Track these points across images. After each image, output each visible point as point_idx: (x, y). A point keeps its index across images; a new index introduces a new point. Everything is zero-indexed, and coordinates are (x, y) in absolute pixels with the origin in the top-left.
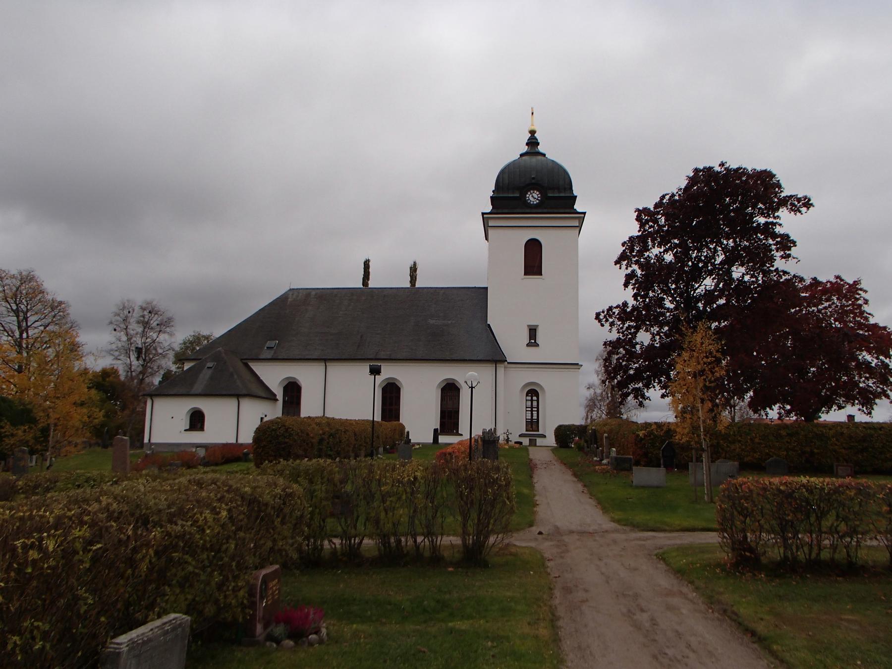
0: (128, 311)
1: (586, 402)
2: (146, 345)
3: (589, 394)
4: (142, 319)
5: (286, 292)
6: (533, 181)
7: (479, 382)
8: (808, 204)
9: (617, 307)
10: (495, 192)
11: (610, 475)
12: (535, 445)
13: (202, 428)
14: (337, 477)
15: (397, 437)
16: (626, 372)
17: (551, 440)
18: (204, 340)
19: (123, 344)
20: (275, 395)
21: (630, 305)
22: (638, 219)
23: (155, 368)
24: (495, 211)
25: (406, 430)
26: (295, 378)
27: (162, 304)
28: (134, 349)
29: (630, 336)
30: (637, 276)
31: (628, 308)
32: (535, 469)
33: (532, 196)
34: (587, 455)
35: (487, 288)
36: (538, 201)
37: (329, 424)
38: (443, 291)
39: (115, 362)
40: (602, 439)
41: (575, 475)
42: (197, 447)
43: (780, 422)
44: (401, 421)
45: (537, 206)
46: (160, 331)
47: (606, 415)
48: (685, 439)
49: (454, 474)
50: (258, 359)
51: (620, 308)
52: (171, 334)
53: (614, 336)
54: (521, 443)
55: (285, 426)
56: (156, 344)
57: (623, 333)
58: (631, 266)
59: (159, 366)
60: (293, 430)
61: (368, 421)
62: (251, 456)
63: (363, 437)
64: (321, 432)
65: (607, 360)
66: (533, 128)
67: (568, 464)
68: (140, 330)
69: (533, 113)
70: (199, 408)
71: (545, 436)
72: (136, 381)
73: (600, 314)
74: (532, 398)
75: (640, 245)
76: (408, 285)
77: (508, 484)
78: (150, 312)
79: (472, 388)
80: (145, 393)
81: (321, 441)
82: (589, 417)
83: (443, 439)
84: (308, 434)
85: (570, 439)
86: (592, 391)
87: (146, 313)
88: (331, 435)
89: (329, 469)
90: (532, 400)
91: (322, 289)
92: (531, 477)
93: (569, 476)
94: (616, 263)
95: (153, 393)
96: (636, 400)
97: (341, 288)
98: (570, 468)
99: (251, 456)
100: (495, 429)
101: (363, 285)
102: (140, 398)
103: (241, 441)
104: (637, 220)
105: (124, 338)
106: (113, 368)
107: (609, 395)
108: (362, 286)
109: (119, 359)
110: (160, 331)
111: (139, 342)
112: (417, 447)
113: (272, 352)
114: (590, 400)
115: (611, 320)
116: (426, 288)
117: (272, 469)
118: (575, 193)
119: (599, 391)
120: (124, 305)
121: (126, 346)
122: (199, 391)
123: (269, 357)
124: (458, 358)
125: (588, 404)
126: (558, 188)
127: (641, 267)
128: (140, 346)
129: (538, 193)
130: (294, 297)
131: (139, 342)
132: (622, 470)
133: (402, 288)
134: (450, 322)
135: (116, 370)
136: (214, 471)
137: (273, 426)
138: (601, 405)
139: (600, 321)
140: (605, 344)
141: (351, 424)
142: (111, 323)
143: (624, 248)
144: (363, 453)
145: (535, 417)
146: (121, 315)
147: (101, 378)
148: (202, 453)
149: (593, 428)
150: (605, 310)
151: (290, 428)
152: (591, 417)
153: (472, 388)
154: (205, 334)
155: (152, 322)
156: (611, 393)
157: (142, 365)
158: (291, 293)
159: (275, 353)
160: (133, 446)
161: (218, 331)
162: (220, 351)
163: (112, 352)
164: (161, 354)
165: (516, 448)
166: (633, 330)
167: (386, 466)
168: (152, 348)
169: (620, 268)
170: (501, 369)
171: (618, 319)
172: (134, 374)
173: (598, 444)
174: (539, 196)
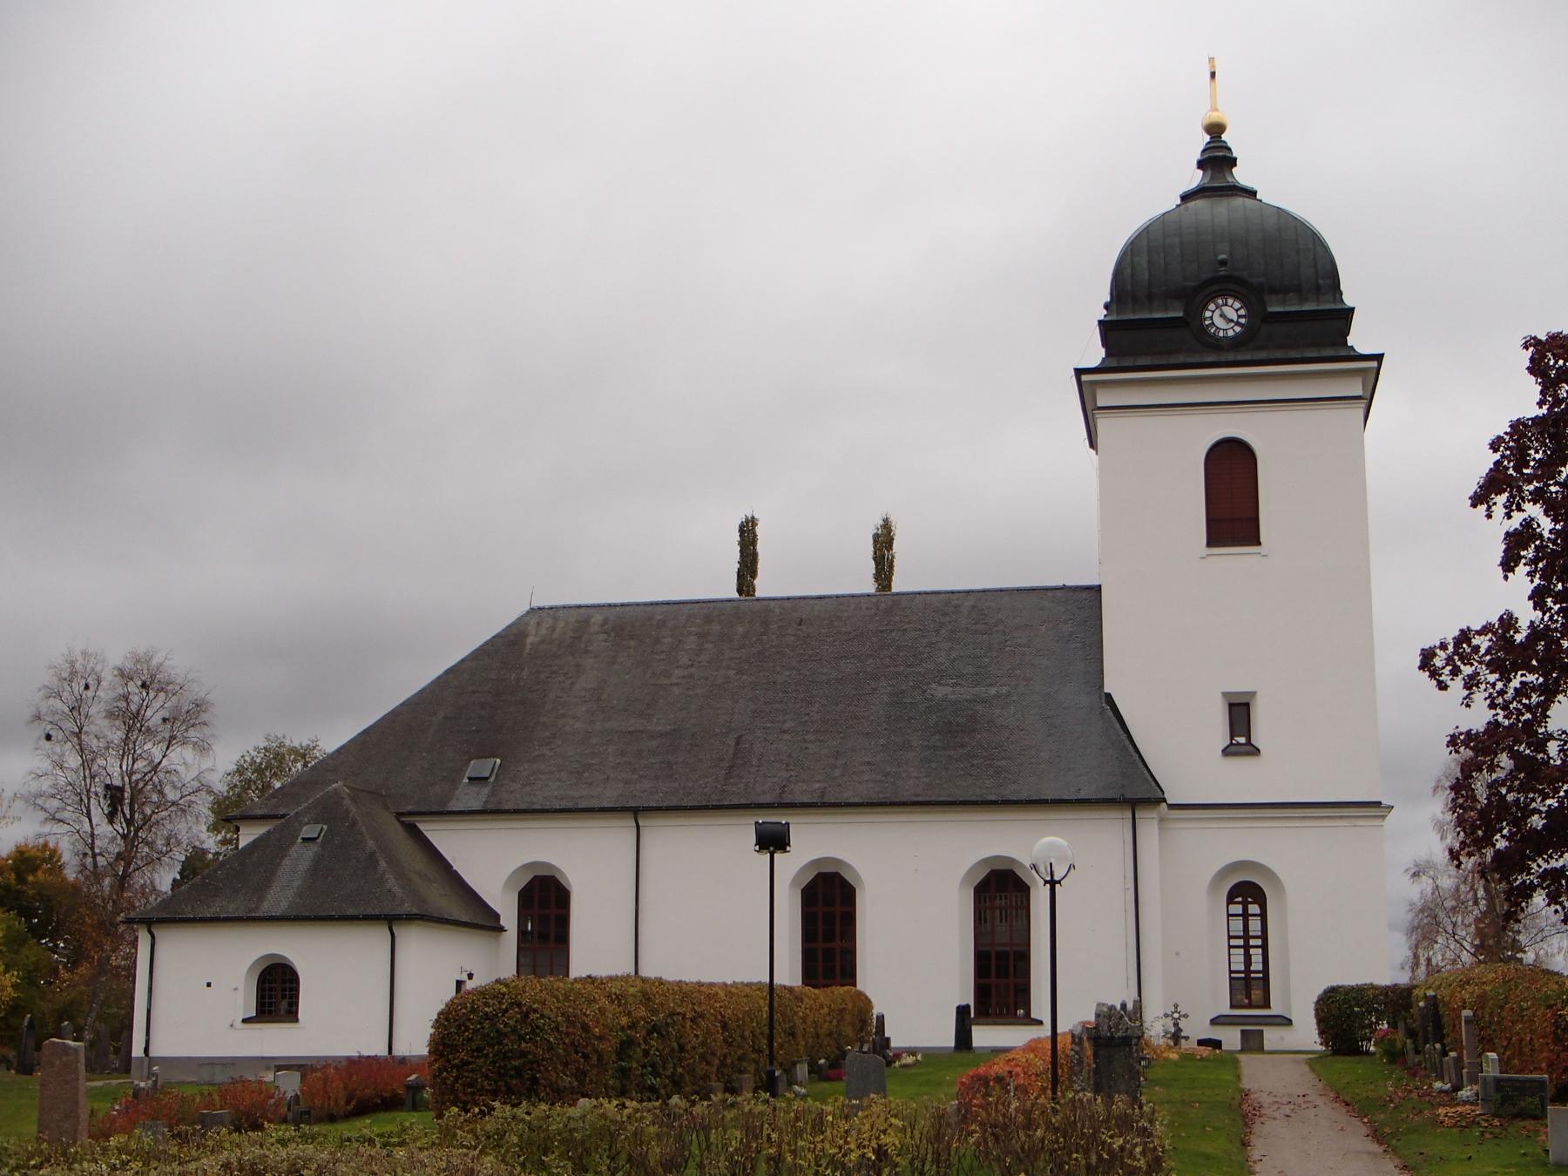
0: (83, 682)
1: (1410, 916)
2: (134, 778)
3: (1416, 891)
4: (123, 704)
5: (519, 619)
6: (1223, 271)
7: (1071, 867)
9: (1483, 631)
10: (1114, 307)
11: (1482, 1134)
12: (1260, 1049)
13: (291, 1015)
14: (655, 1152)
15: (849, 1031)
16: (1518, 823)
17: (1306, 1033)
18: (295, 761)
19: (71, 777)
20: (497, 917)
21: (1523, 624)
22: (1536, 368)
23: (160, 843)
24: (1113, 363)
25: (875, 1012)
27: (177, 663)
28: (100, 790)
29: (1528, 716)
30: (1541, 536)
31: (1517, 631)
32: (1258, 1121)
33: (1223, 316)
34: (1414, 1075)
35: (1098, 589)
36: (1238, 329)
37: (646, 998)
39: (47, 829)
40: (1455, 1027)
41: (1377, 1135)
42: (279, 1068)
43: (1490, 974)
44: (860, 987)
45: (1236, 343)
46: (173, 737)
47: (1474, 955)
49: (996, 1138)
50: (443, 814)
51: (1494, 634)
52: (202, 748)
53: (1478, 717)
54: (1216, 1044)
55: (519, 1005)
56: (161, 775)
57: (1505, 707)
58: (1519, 509)
59: (168, 839)
60: (542, 1016)
61: (759, 986)
62: (427, 1094)
63: (747, 1033)
64: (624, 1021)
65: (1461, 787)
66: (1215, 117)
67: (1355, 1105)
68: (117, 736)
69: (1213, 75)
71: (1288, 1022)
72: (107, 881)
73: (1435, 655)
74: (1245, 909)
75: (1543, 444)
76: (869, 587)
78: (144, 685)
79: (1053, 883)
80: (132, 915)
81: (625, 1047)
82: (1423, 961)
83: (984, 1036)
84: (585, 1028)
85: (1364, 1027)
86: (1426, 884)
87: (133, 688)
88: (655, 1028)
89: (631, 1128)
90: (1245, 915)
91: (622, 605)
92: (1245, 1145)
93: (1356, 1138)
94: (1476, 500)
95: (155, 915)
96: (1553, 908)
97: (675, 603)
98: (1361, 1115)
99: (427, 1094)
100: (1139, 1005)
101: (740, 591)
102: (122, 928)
103: (401, 1050)
104: (1531, 370)
105: (73, 761)
106: (46, 845)
107: (1481, 893)
108: (736, 595)
109: (60, 821)
110: (173, 737)
111: (115, 771)
112: (910, 1060)
113: (486, 790)
114: (1422, 911)
115: (1467, 670)
116: (920, 593)
117: (472, 1131)
118: (1349, 301)
119: (1447, 882)
120: (72, 664)
121: (80, 783)
123: (476, 806)
124: (1024, 796)
125: (1416, 923)
126: (1297, 289)
127: (1551, 509)
128: (117, 782)
129: (1237, 305)
130: (544, 631)
131: (115, 771)
132: (1516, 1116)
133: (853, 596)
134: (993, 691)
135: (54, 852)
136: (306, 1139)
137: (486, 1005)
138: (1454, 925)
139: (1435, 674)
140: (1453, 741)
141: (712, 997)
143: (1497, 456)
144: (748, 1079)
145: (1257, 965)
146: (65, 695)
147: (13, 876)
148: (290, 1085)
149: (1431, 993)
150: (1450, 640)
151: (535, 1011)
152: (1429, 960)
154: (296, 744)
155: (149, 713)
156: (1486, 890)
157: (124, 837)
158: (533, 622)
159: (493, 793)
160: (96, 1066)
161: (332, 738)
163: (39, 801)
164: (174, 803)
165: (1202, 1059)
166: (1535, 699)
167: (797, 1119)
168: (149, 787)
169: (1489, 516)
170: (1149, 825)
171: (1488, 665)
172: (101, 861)
173: (1447, 1040)
174: (1242, 312)
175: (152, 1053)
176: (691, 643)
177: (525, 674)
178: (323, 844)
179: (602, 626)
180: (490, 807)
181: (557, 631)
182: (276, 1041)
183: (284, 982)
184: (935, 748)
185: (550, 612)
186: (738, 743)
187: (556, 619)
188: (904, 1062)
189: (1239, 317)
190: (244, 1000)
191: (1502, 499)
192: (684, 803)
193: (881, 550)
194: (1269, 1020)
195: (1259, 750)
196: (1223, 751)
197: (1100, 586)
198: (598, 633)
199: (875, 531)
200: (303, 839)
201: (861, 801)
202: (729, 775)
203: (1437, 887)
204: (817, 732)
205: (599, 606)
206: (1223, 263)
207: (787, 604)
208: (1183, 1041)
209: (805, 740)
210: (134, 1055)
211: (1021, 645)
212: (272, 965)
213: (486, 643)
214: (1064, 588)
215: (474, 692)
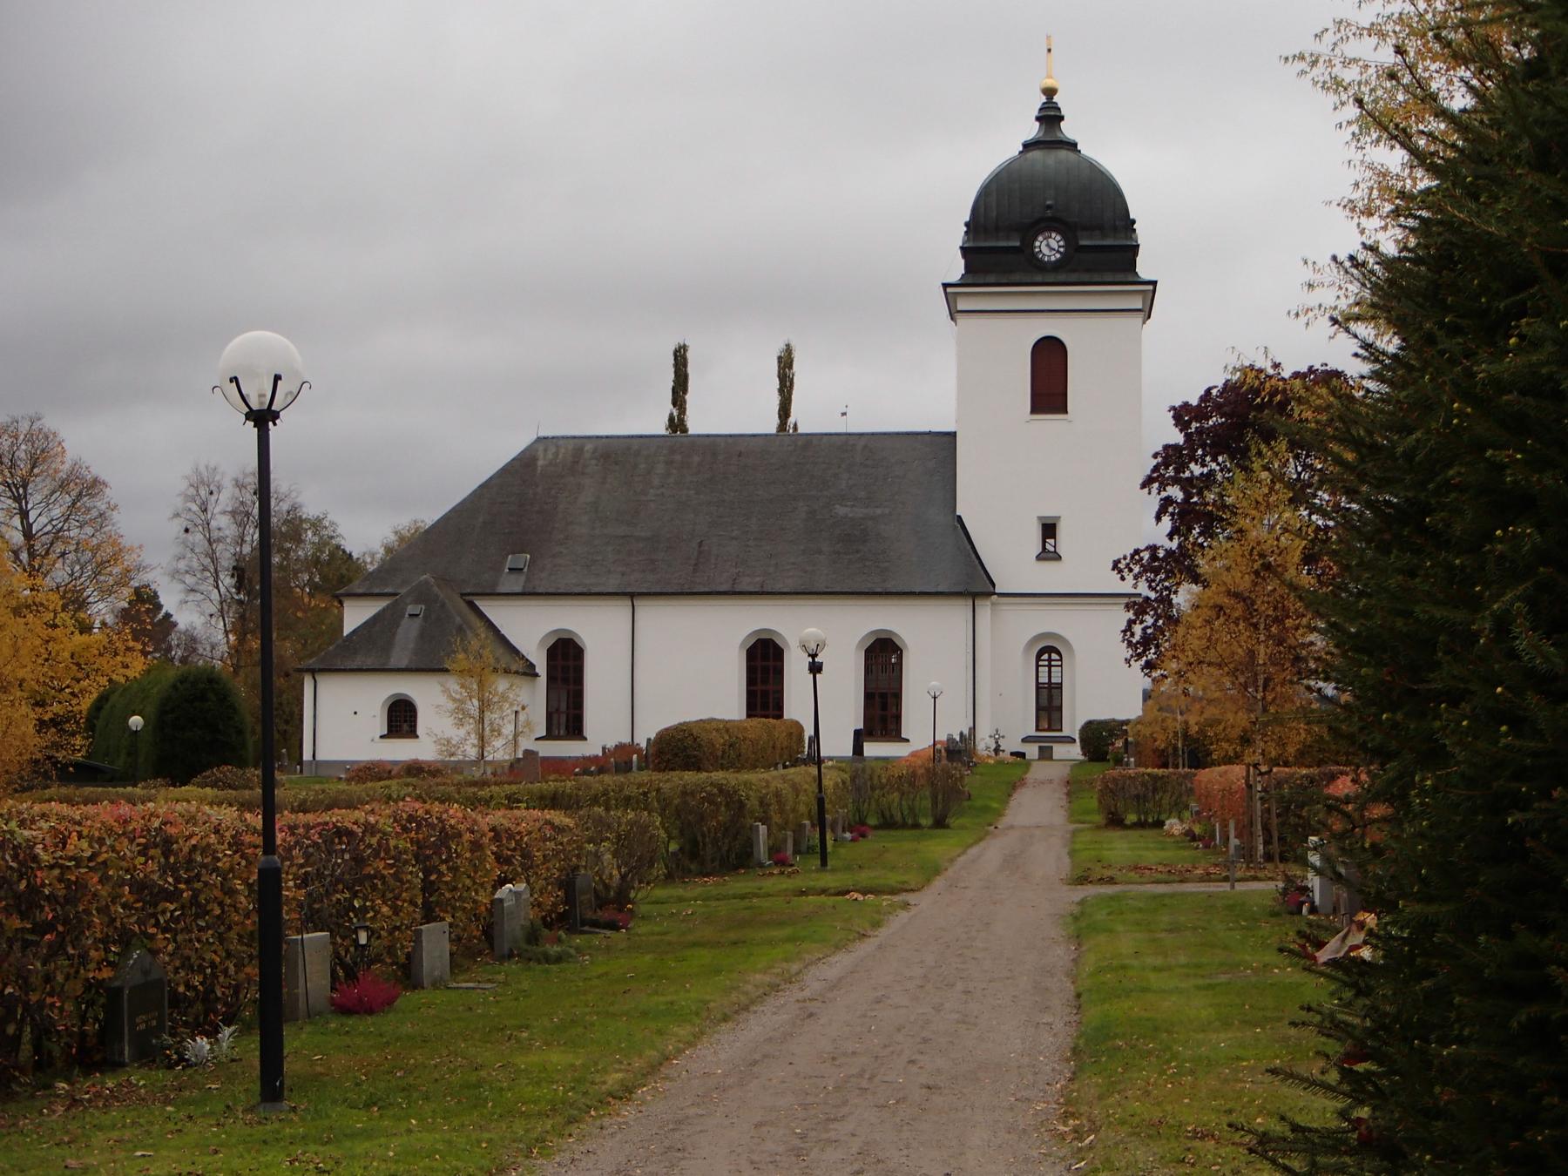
6: (1049, 213)
12: (1051, 758)
13: (412, 733)
17: (1075, 752)
20: (532, 666)
26: (570, 632)
33: (1048, 245)
35: (953, 435)
36: (1058, 256)
45: (1057, 267)
48: (1163, 746)
54: (1022, 755)
58: (1165, 490)
66: (1050, 83)
69: (1049, 50)
70: (406, 695)
74: (1050, 656)
79: (935, 698)
83: (872, 749)
91: (607, 437)
92: (1010, 796)
94: (1143, 486)
97: (646, 436)
112: (830, 763)
113: (522, 578)
116: (826, 434)
122: (403, 664)
123: (518, 589)
124: (899, 589)
129: (1058, 238)
130: (550, 456)
134: (879, 511)
139: (1120, 571)
142: (177, 515)
153: (935, 698)
159: (528, 580)
162: (426, 582)
169: (1150, 493)
170: (985, 609)
175: (317, 759)
176: (660, 468)
177: (539, 490)
178: (426, 618)
180: (527, 590)
181: (560, 456)
183: (406, 711)
184: (838, 553)
186: (700, 546)
189: (1059, 247)
191: (1156, 485)
192: (664, 591)
193: (784, 370)
197: (955, 433)
200: (410, 615)
202: (695, 571)
204: (755, 539)
205: (589, 438)
206: (1049, 207)
207: (730, 440)
209: (748, 546)
210: (305, 759)
213: (507, 465)
215: (502, 503)
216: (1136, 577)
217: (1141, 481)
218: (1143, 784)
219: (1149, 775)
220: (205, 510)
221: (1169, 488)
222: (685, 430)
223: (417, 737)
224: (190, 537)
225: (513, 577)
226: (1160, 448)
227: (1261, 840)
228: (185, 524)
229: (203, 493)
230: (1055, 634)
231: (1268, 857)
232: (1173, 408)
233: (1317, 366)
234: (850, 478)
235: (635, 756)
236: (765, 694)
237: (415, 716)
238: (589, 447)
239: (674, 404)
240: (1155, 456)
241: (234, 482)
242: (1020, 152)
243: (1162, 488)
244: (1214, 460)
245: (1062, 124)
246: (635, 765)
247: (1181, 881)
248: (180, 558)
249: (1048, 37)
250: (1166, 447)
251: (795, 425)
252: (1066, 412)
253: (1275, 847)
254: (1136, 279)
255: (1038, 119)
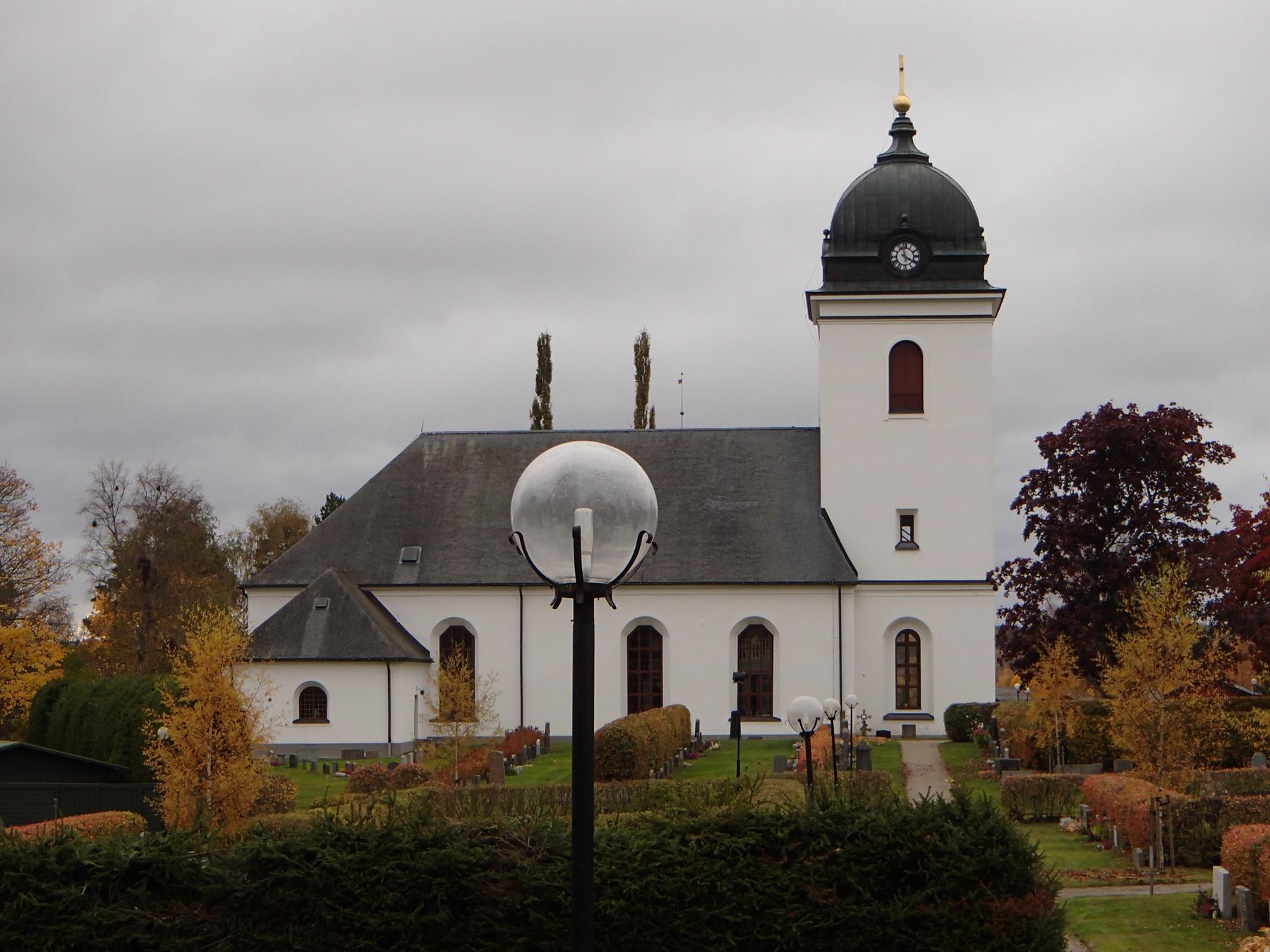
8: (1229, 453)
13: (322, 718)
17: (938, 727)
20: (428, 653)
26: (463, 620)
33: (904, 255)
35: (818, 429)
36: (913, 265)
38: (729, 438)
45: (912, 275)
54: (886, 734)
58: (1032, 510)
66: (902, 100)
69: (902, 69)
77: (890, 782)
79: (852, 708)
91: (488, 433)
92: (904, 785)
94: (1013, 507)
112: (717, 745)
116: (695, 430)
123: (413, 581)
129: (913, 248)
130: (435, 452)
134: (748, 504)
142: (85, 510)
153: (852, 708)
158: (426, 444)
159: (421, 572)
162: (330, 575)
165: (881, 745)
169: (1019, 513)
170: (849, 596)
174: (916, 253)
179: (476, 449)
182: (312, 734)
183: (316, 698)
185: (437, 437)
187: (442, 443)
188: (714, 747)
189: (914, 256)
190: (293, 711)
191: (1024, 506)
194: (921, 717)
195: (918, 547)
196: (896, 547)
198: (474, 455)
199: (636, 343)
200: (317, 607)
201: (668, 581)
203: (1050, 605)
205: (472, 433)
206: (905, 220)
208: (868, 731)
211: (765, 471)
212: (308, 688)
214: (793, 428)
215: (393, 497)
216: (1007, 587)
217: (1011, 503)
218: (1040, 787)
219: (1043, 779)
220: (111, 506)
221: (1036, 509)
222: (549, 419)
223: (328, 722)
224: (97, 531)
225: (407, 568)
226: (1027, 473)
227: (1162, 852)
228: (92, 518)
229: (108, 489)
230: (909, 618)
231: (1167, 863)
232: (1039, 439)
233: (1167, 405)
234: (719, 472)
235: (538, 741)
236: (645, 676)
237: (325, 703)
238: (472, 443)
239: (539, 392)
240: (1023, 480)
241: (138, 479)
242: (876, 166)
243: (1030, 508)
244: (1077, 484)
245: (914, 137)
246: (538, 749)
247: (1110, 885)
248: (86, 551)
249: (901, 57)
250: (1033, 473)
251: (653, 410)
252: (921, 410)
253: (1173, 856)
254: (986, 288)
255: (891, 133)
